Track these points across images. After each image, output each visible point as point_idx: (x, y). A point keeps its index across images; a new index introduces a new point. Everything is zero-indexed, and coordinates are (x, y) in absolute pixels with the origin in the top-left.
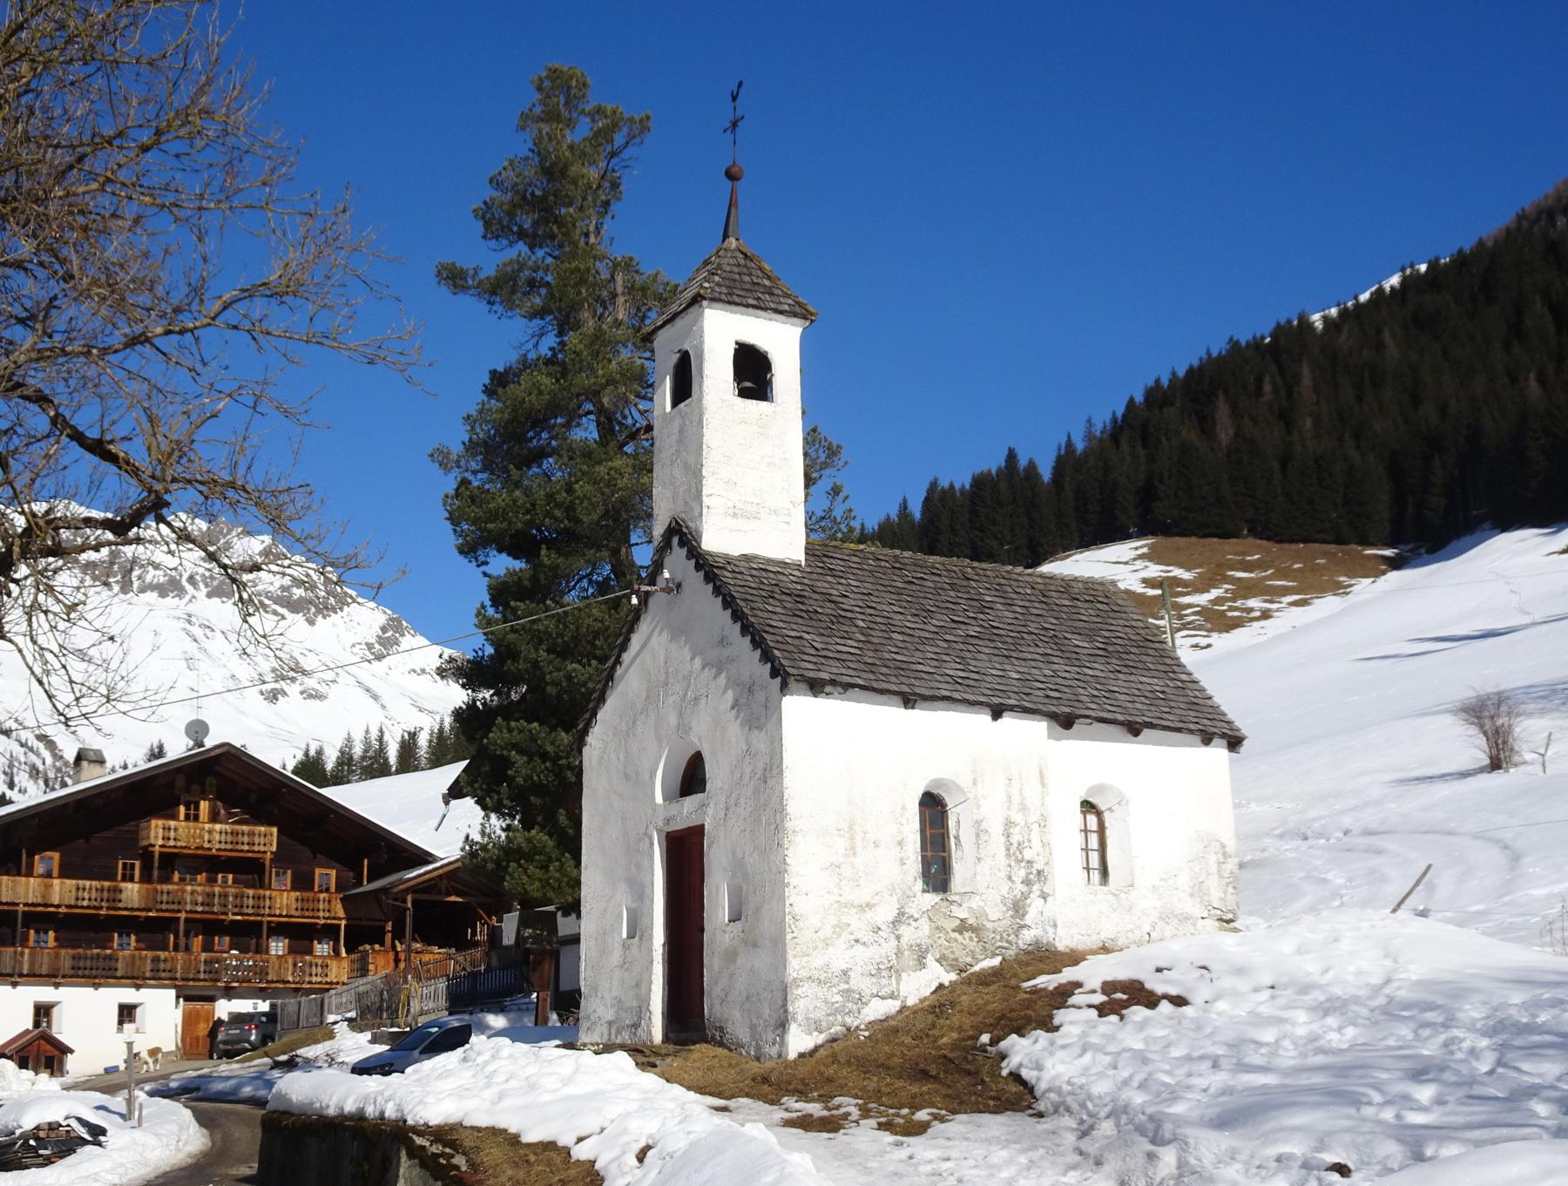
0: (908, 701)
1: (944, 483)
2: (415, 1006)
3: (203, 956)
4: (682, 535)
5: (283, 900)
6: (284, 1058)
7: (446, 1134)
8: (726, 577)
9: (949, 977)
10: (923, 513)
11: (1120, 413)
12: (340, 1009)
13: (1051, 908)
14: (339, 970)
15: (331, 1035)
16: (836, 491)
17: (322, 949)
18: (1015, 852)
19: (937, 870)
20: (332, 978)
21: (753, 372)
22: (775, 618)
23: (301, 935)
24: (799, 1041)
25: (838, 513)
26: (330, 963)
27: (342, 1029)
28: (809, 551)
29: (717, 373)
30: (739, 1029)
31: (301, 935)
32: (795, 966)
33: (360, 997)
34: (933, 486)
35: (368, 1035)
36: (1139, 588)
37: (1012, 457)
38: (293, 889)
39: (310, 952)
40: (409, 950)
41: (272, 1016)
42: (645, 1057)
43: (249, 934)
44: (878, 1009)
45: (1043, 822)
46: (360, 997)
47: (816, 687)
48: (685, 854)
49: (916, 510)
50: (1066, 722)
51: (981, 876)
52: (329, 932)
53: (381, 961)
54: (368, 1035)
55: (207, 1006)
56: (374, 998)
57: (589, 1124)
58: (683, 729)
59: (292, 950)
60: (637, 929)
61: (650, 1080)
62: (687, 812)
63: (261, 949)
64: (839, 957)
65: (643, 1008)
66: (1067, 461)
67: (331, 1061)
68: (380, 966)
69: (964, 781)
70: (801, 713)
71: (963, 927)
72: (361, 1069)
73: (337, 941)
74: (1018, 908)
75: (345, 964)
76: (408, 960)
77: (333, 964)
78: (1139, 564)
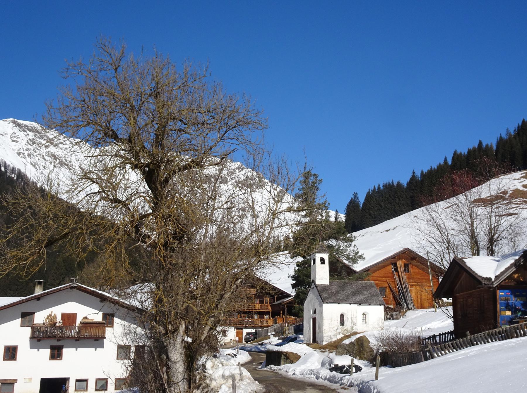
0: (339, 303)
1: (458, 152)
2: (287, 332)
3: (240, 319)
4: (314, 281)
5: (258, 306)
6: (261, 343)
7: (286, 353)
8: (318, 288)
9: (343, 336)
10: (452, 162)
11: (520, 124)
12: (271, 332)
13: (357, 327)
14: (270, 322)
15: (269, 338)
16: (355, 246)
17: (266, 317)
18: (352, 321)
19: (342, 323)
20: (269, 324)
21: (322, 261)
22: (324, 294)
23: (261, 314)
24: (325, 343)
25: (355, 249)
26: (268, 320)
27: (272, 336)
28: (330, 282)
29: (318, 261)
30: (319, 342)
31: (261, 314)
32: (324, 335)
33: (275, 330)
34: (455, 153)
35: (277, 338)
36: (521, 188)
37: (480, 143)
38: (260, 303)
39: (264, 318)
40: (286, 318)
41: (256, 333)
42: (308, 345)
43: (249, 313)
44: (334, 340)
45: (356, 317)
46: (275, 330)
47: (327, 303)
48: (314, 320)
49: (450, 162)
50: (360, 304)
51: (348, 324)
52: (268, 313)
53: (280, 320)
54: (277, 338)
55: (241, 330)
56: (278, 330)
57: (300, 351)
58: (314, 306)
59: (259, 318)
60: (310, 329)
61: (308, 347)
62: (314, 316)
63: (253, 318)
64: (329, 334)
65: (310, 339)
66: (501, 142)
67: (270, 344)
68: (280, 321)
69: (346, 312)
70: (325, 305)
71: (345, 330)
72: (277, 345)
73: (269, 315)
74: (352, 327)
75: (272, 321)
76: (286, 320)
77: (269, 321)
78: (522, 180)
